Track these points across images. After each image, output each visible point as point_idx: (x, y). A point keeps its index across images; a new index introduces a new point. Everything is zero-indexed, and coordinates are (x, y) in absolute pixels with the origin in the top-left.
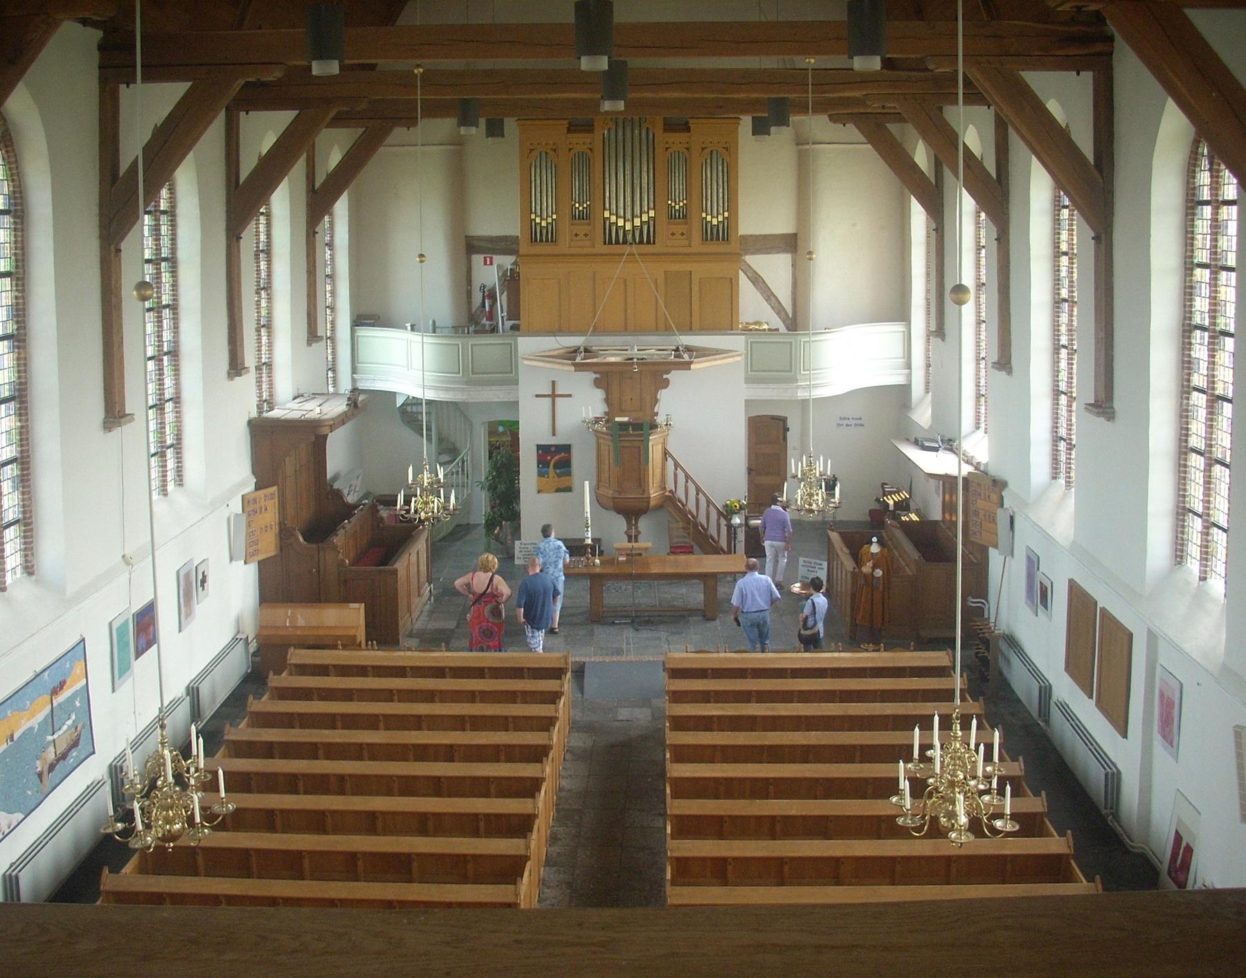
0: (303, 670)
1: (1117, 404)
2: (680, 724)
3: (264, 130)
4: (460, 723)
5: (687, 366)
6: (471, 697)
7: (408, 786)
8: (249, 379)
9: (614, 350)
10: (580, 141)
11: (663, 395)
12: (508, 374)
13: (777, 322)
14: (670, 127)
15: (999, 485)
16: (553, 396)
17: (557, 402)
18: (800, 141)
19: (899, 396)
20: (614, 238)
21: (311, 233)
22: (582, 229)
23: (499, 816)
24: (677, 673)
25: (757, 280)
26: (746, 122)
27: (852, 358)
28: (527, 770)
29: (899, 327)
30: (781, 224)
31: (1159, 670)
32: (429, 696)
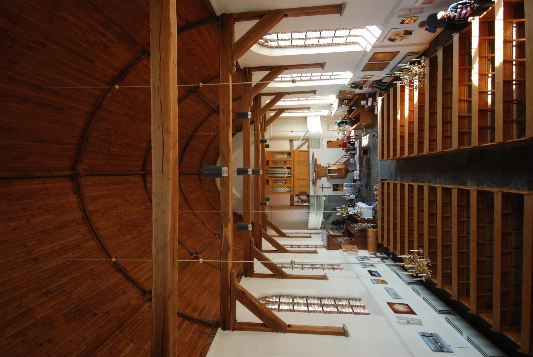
0: (383, 239)
1: (322, 62)
2: (395, 154)
3: (266, 245)
4: (395, 204)
5: (316, 159)
6: (389, 202)
7: (411, 214)
8: (318, 250)
9: (312, 175)
10: (270, 182)
11: (322, 165)
12: (318, 197)
13: (307, 144)
14: (267, 164)
15: (341, 92)
16: (322, 188)
17: (324, 188)
18: (270, 139)
19: (323, 117)
20: (290, 175)
21: (288, 237)
22: (288, 182)
23: (418, 193)
24: (383, 157)
25: (299, 147)
26: (266, 149)
27: (315, 126)
28: (406, 188)
29: (308, 118)
30: (288, 143)
31: (383, 44)
32: (389, 211)
